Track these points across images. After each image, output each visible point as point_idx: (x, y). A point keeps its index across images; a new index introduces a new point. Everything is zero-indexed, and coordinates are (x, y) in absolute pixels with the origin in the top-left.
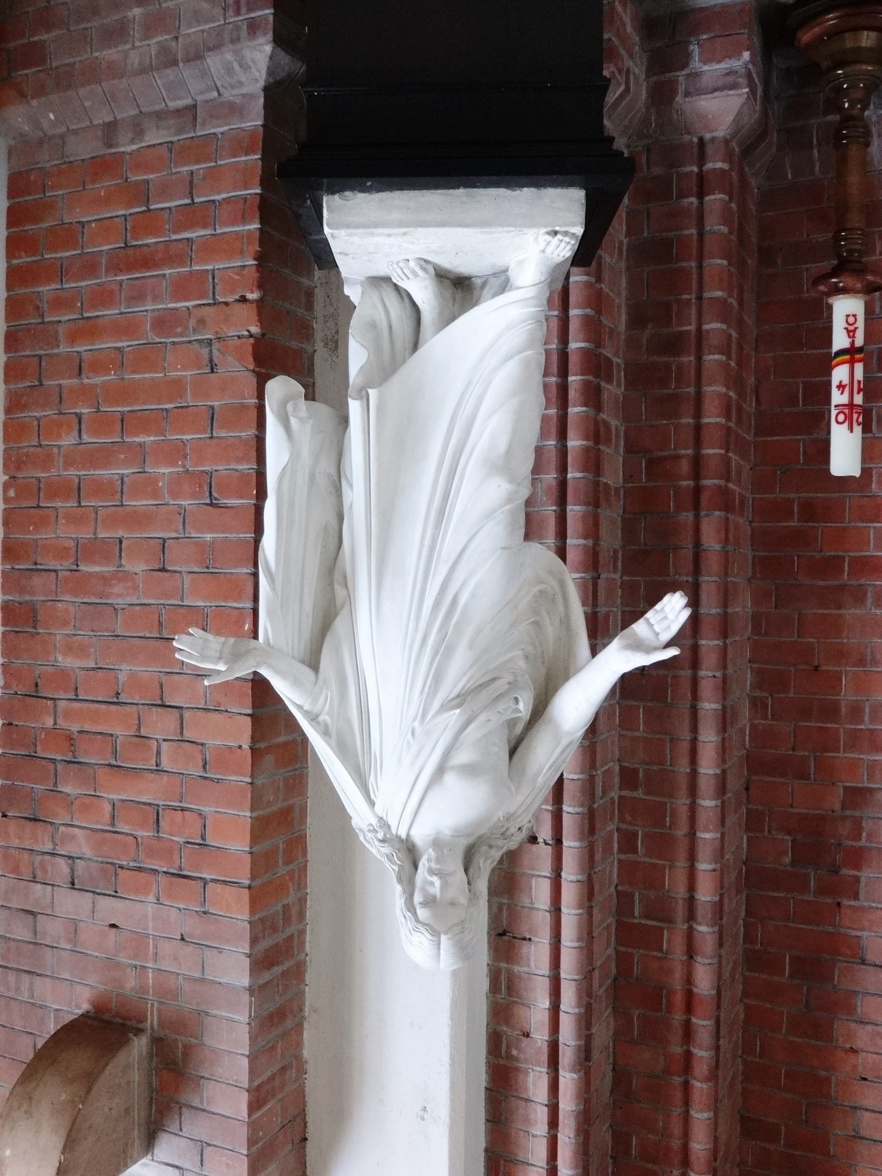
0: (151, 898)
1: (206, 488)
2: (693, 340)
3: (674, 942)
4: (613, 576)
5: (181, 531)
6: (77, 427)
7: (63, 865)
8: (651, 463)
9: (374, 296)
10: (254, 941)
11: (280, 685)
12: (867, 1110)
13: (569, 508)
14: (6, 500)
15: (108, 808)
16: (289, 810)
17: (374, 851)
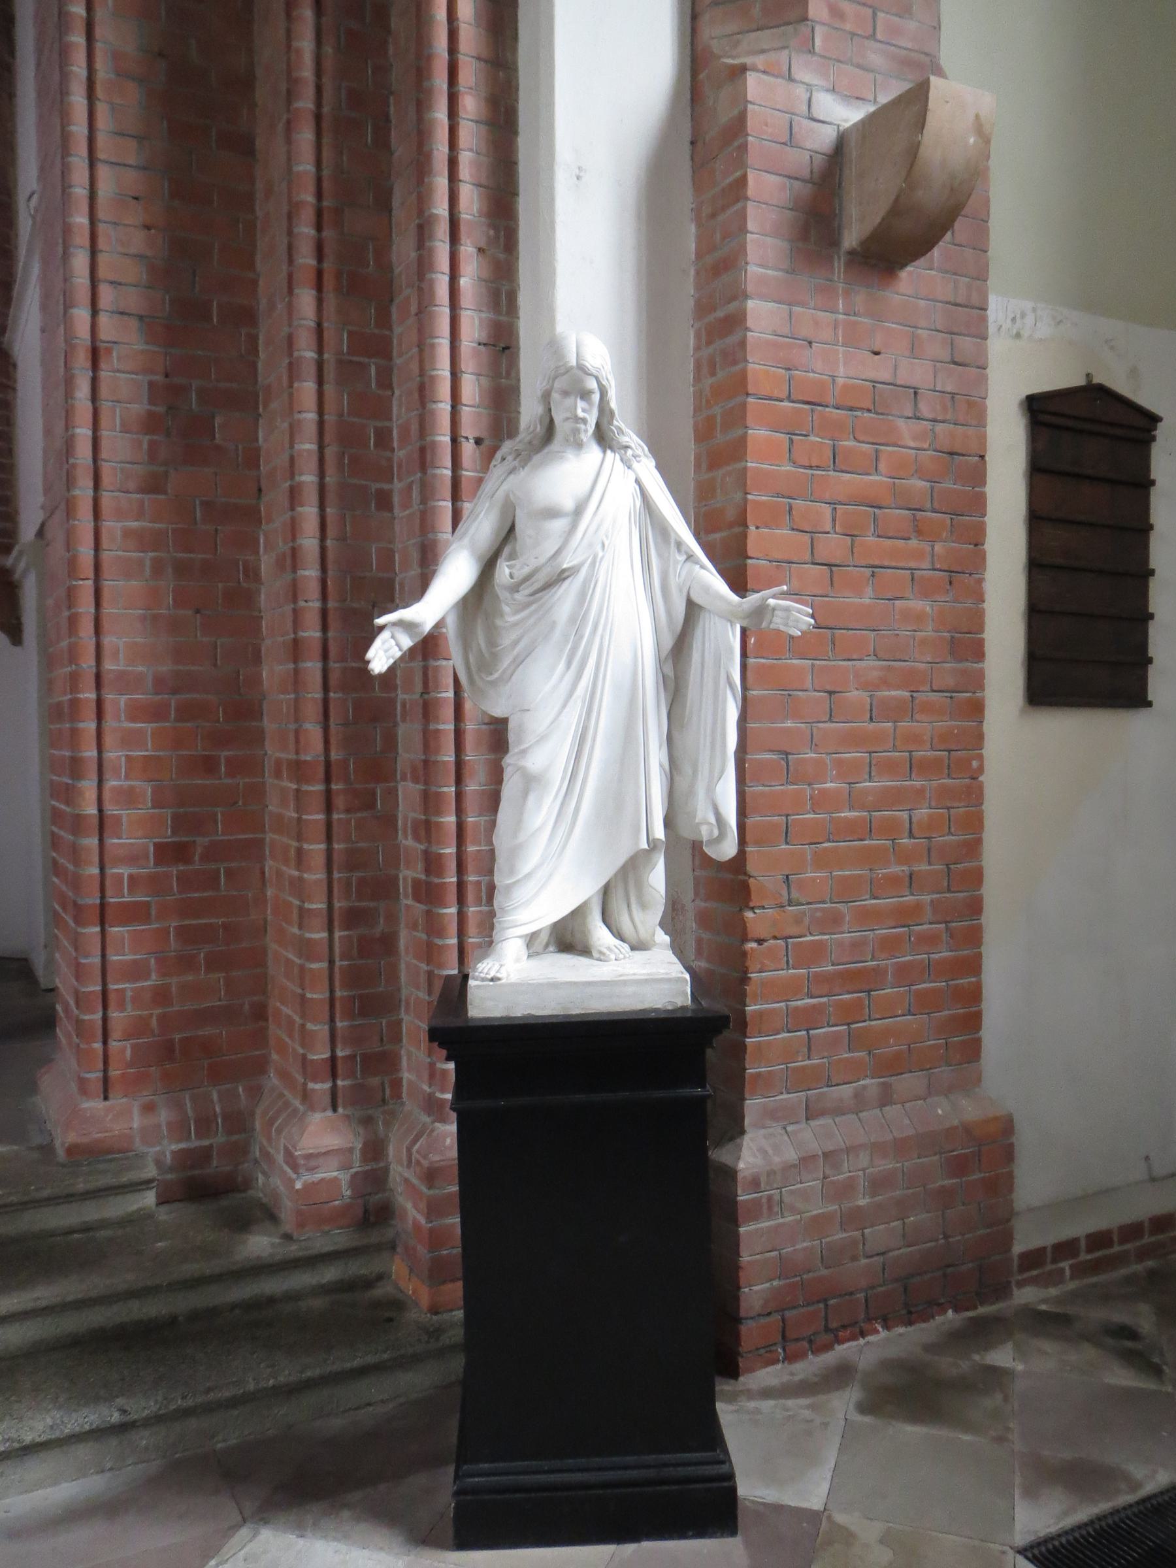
0: (840, 381)
1: (791, 768)
2: (336, 923)
3: (338, 341)
4: (405, 696)
5: (815, 730)
6: (914, 826)
7: (925, 410)
8: (371, 806)
9: (643, 934)
10: (743, 344)
11: (721, 586)
12: (130, 166)
13: (453, 759)
14: (980, 758)
15: (882, 466)
16: (713, 465)
17: (635, 437)
